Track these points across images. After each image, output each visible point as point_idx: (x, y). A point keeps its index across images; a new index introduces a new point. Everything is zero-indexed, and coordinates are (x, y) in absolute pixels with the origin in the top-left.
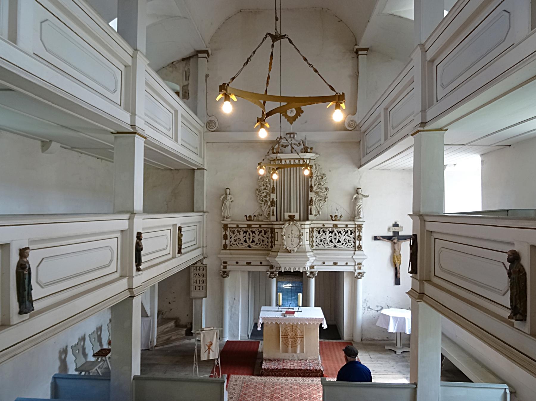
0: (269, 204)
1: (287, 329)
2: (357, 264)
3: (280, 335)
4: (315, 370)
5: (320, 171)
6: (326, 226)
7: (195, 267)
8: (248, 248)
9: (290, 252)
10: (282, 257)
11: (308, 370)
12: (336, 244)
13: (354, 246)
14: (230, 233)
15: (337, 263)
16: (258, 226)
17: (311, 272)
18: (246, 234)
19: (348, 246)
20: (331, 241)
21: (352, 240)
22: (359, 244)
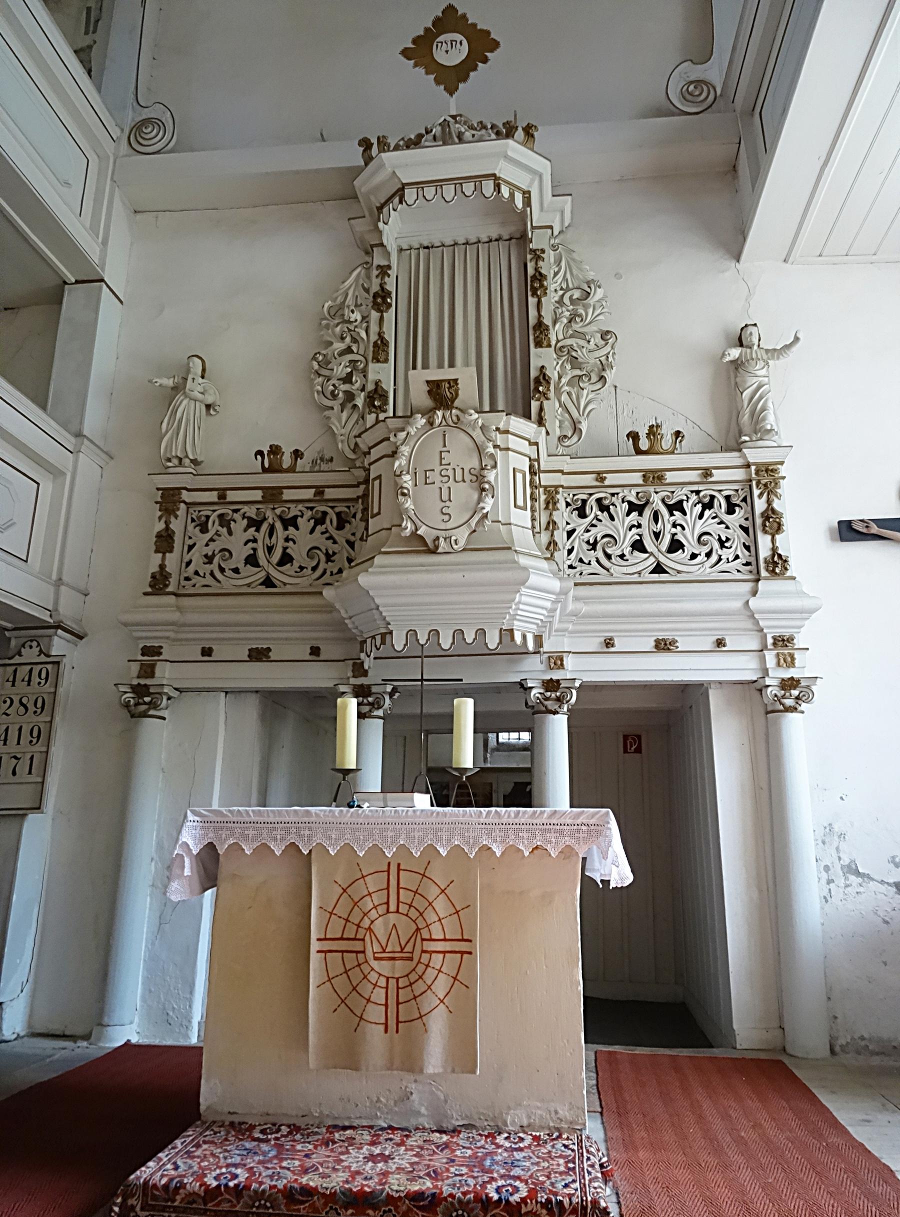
0: (360, 401)
1: (360, 889)
2: (770, 641)
3: (314, 936)
4: (547, 1204)
5: (575, 272)
6: (610, 479)
7: (11, 669)
8: (263, 589)
9: (434, 551)
10: (385, 570)
11: (486, 1203)
12: (662, 559)
13: (748, 564)
14: (191, 527)
15: (673, 642)
16: (309, 494)
17: (551, 685)
18: (258, 530)
19: (722, 566)
20: (638, 546)
21: (738, 538)
22: (774, 550)
